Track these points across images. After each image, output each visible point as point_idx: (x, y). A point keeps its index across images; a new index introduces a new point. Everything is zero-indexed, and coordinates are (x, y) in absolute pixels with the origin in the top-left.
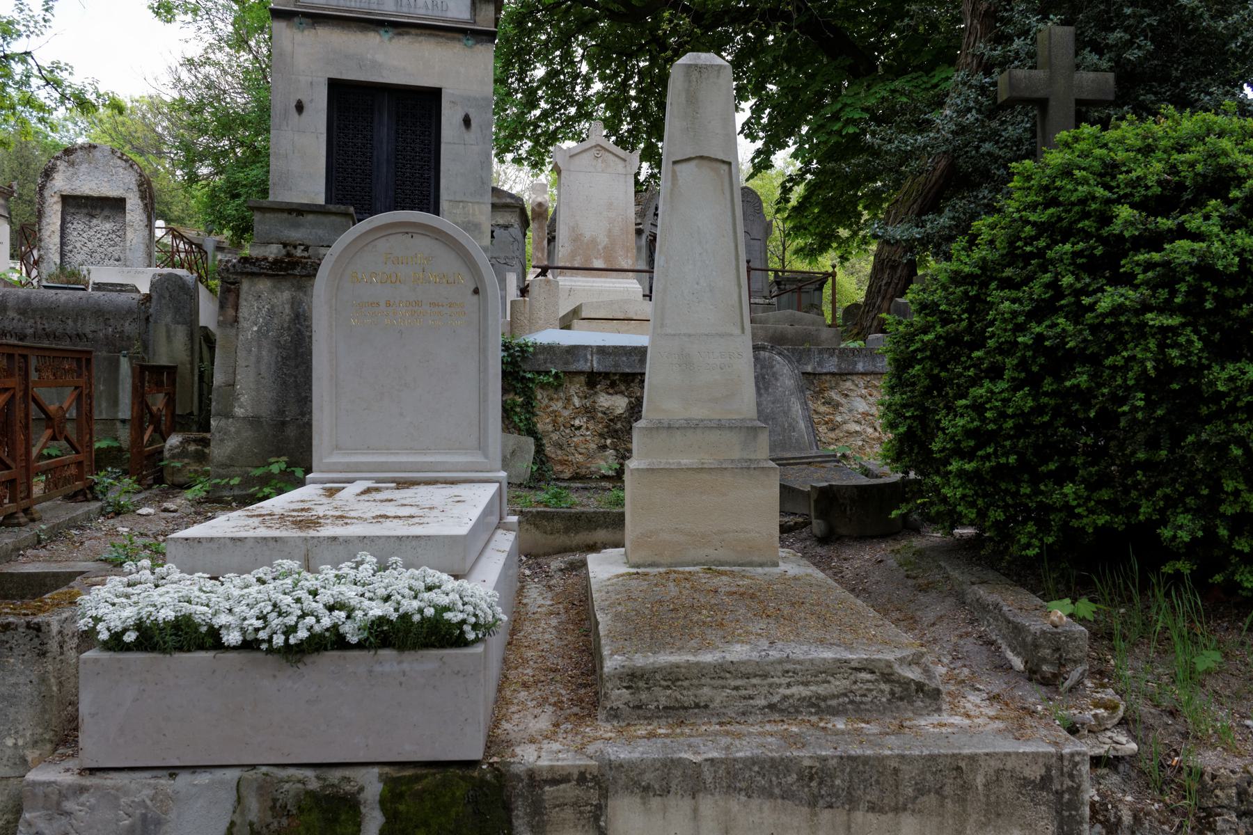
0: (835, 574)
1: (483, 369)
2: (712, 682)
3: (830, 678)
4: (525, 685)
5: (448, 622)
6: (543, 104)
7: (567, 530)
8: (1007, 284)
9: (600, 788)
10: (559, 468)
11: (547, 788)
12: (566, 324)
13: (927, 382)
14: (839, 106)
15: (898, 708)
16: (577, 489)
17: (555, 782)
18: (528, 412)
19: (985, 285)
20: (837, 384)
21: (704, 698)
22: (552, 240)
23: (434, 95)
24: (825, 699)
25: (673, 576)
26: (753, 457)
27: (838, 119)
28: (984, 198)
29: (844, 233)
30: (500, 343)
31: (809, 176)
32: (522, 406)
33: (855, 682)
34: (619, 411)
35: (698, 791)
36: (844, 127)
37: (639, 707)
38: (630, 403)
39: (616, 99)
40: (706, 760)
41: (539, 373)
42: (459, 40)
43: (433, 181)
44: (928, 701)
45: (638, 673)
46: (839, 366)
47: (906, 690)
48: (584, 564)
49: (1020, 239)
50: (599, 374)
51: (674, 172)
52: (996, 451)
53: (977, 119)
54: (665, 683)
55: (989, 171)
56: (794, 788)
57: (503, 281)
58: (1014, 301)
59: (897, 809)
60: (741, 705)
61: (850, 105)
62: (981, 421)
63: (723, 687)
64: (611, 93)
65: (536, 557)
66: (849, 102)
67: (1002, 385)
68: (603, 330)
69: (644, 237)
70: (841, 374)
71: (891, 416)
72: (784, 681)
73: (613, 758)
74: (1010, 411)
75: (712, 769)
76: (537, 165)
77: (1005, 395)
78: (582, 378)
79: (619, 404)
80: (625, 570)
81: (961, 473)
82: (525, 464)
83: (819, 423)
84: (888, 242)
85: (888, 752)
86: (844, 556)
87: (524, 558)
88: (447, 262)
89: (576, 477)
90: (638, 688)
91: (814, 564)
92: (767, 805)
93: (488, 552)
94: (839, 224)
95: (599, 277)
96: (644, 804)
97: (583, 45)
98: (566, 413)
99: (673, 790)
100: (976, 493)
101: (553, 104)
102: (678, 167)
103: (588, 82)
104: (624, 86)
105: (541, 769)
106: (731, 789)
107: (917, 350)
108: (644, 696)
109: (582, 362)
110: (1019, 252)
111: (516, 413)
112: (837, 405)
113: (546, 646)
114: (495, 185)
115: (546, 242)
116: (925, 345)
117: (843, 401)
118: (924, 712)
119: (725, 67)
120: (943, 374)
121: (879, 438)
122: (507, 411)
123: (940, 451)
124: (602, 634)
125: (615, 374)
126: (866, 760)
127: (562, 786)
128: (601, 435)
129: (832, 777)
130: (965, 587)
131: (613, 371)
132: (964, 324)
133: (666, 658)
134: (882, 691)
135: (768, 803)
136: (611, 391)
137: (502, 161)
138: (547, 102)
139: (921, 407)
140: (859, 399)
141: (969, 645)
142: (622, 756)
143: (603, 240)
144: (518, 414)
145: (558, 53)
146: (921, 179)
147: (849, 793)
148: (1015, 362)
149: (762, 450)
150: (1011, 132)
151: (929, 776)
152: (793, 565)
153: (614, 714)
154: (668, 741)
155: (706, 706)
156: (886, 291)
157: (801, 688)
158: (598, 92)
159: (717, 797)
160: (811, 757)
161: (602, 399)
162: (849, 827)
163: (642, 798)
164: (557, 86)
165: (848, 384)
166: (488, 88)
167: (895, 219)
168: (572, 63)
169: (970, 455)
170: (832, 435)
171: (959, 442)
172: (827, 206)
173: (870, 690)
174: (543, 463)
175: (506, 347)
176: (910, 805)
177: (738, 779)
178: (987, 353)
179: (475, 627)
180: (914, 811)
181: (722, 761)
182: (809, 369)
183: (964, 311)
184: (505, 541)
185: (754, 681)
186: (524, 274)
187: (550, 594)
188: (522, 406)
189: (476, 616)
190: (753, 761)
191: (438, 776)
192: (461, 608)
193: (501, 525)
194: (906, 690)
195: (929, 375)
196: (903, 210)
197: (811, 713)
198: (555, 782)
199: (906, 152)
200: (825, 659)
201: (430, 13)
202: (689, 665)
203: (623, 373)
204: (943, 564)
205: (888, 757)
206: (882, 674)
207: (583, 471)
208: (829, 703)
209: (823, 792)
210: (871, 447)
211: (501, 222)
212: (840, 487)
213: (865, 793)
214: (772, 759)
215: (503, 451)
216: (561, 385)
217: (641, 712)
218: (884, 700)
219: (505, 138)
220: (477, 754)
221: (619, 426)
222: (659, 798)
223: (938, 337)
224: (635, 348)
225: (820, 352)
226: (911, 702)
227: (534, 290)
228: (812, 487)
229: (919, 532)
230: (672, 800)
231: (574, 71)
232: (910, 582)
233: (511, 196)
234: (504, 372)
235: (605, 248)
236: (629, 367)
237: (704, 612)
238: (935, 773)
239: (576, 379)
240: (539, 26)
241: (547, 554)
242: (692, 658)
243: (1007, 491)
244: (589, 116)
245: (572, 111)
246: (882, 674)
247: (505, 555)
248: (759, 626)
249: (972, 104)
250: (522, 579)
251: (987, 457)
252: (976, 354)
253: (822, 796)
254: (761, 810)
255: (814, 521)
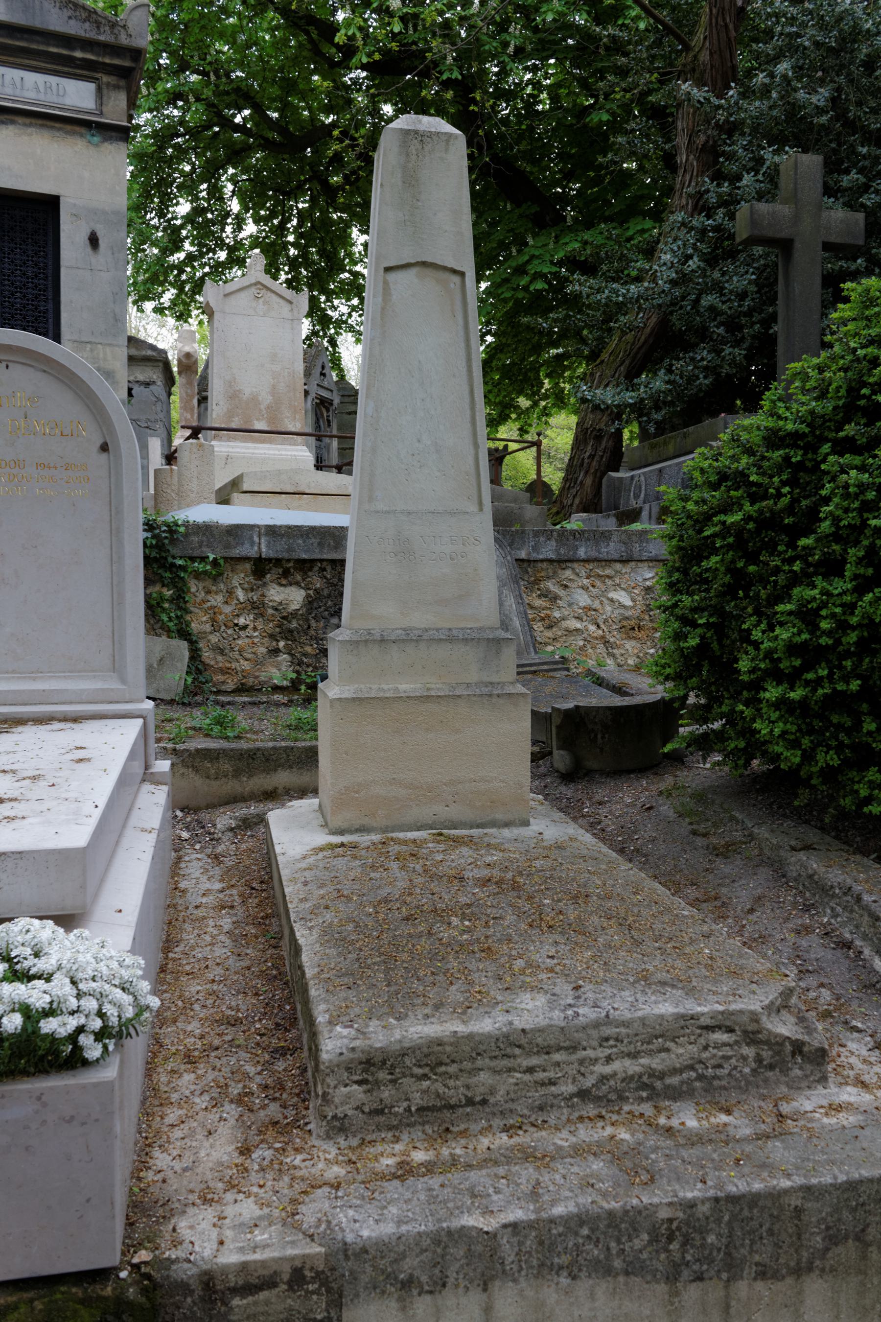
0: (592, 825)
1: (116, 558)
2: (493, 1064)
3: (670, 1044)
4: (190, 1059)
5: (52, 1038)
6: (187, 246)
7: (237, 774)
8: (845, 446)
9: (329, 1290)
10: (220, 678)
11: (236, 1302)
12: (223, 498)
13: (727, 579)
14: (526, 258)
15: (766, 1081)
16: (244, 705)
17: (249, 1289)
18: (180, 608)
19: (812, 448)
20: (555, 573)
21: (482, 1089)
22: (203, 400)
23: (50, 205)
24: (662, 1076)
25: (394, 849)
26: (495, 679)
27: (525, 272)
28: (702, 359)
29: (524, 402)
30: (141, 521)
31: (489, 339)
32: (171, 601)
33: (706, 1048)
34: (294, 606)
35: (493, 1278)
36: (531, 282)
37: (379, 1112)
38: (308, 596)
39: (273, 244)
40: (505, 1226)
41: (193, 559)
42: (82, 136)
43: (51, 316)
44: (809, 1067)
45: (378, 1059)
46: (557, 551)
47: (778, 1053)
48: (262, 820)
49: (865, 384)
50: (269, 560)
51: (386, 283)
52: (830, 675)
53: (699, 267)
54: (418, 1071)
55: (705, 329)
56: (645, 1256)
57: (144, 448)
58: (862, 469)
59: (799, 1271)
60: (536, 1095)
61: (538, 257)
62: (812, 633)
63: (510, 1070)
64: (267, 237)
65: (196, 810)
66: (537, 253)
67: (839, 586)
68: (269, 506)
69: (310, 399)
70: (559, 561)
71: (676, 625)
72: (602, 1053)
73: (350, 1238)
74: (854, 620)
75: (515, 1240)
76: (183, 317)
77: (847, 598)
78: (248, 566)
79: (293, 597)
80: (323, 838)
81: (781, 704)
82: (176, 677)
83: (534, 620)
84: (597, 407)
85: (786, 1183)
86: (597, 798)
87: (179, 814)
88: (61, 405)
89: (242, 689)
90: (377, 1083)
91: (561, 810)
92: (602, 1288)
93: (129, 833)
94: (520, 393)
95: (271, 442)
96: (403, 1309)
97: (233, 180)
98: (227, 609)
99: (451, 1281)
100: (800, 730)
101: (200, 245)
102: (392, 277)
103: (239, 224)
104: (281, 229)
105: (225, 1270)
106: (545, 1269)
107: (714, 535)
108: (386, 1093)
109: (247, 545)
110: (862, 402)
111: (164, 610)
112: (555, 598)
113: (219, 970)
114: (133, 333)
115: (195, 402)
116: (726, 529)
117: (561, 593)
118: (804, 1084)
119: (456, 137)
120: (752, 568)
121: (603, 637)
122: (152, 608)
123: (750, 672)
124: (309, 973)
125: (288, 561)
126: (753, 1200)
127: (263, 1295)
128: (272, 636)
129: (703, 1231)
130: (782, 853)
131: (286, 556)
132: (784, 501)
133: (419, 1029)
134: (744, 1058)
135: (604, 1285)
136: (284, 582)
137: (141, 310)
138: (192, 244)
139: (718, 610)
140: (580, 591)
141: (816, 948)
142: (365, 1233)
143: (266, 399)
144: (166, 611)
145: (205, 186)
146: (629, 337)
147: (728, 1254)
148: (861, 553)
149: (505, 669)
150: (737, 283)
151: (846, 1215)
152: (549, 827)
153: (339, 1127)
154: (435, 1182)
155: (484, 1102)
156: (590, 464)
157: (627, 1062)
158: (251, 236)
159: (523, 1284)
160: (670, 1204)
161: (272, 592)
162: (728, 1307)
163: (400, 1299)
164: (204, 225)
165: (568, 573)
166: (121, 201)
167: (600, 383)
168: (221, 199)
169: (792, 679)
170: (549, 634)
171: (779, 660)
172: (506, 372)
173: (727, 1058)
174: (199, 672)
175: (149, 526)
176: (817, 1263)
177: (555, 1250)
178: (817, 540)
179: (99, 1036)
180: (823, 1270)
181: (531, 1225)
182: (523, 555)
183: (784, 483)
184: (153, 804)
185: (557, 1057)
186: (170, 441)
187: (217, 871)
188: (171, 601)
189: (101, 1014)
190: (580, 1219)
191: (39, 1305)
192: (73, 1003)
193: (148, 777)
194: (778, 1053)
195: (731, 570)
196: (608, 373)
197: (642, 1100)
198: (249, 1289)
199: (617, 303)
200: (662, 1017)
201: (42, 97)
202: (457, 1040)
203: (314, 564)
204: (739, 815)
205: (786, 1192)
206: (745, 1032)
207: (250, 681)
208: (668, 1081)
209: (688, 1257)
210: (594, 648)
211: (141, 378)
212: (589, 710)
213: (752, 1251)
214: (611, 1214)
215: (147, 658)
216: (221, 574)
217: (382, 1119)
218: (747, 1070)
219: (145, 282)
220: (115, 1259)
221: (294, 624)
222: (428, 1298)
223: (748, 518)
224: (313, 528)
225: (536, 534)
226: (785, 1071)
227: (183, 457)
228: (553, 708)
229: (683, 763)
230: (449, 1298)
231: (223, 209)
232: (699, 841)
233: (153, 348)
234: (146, 558)
235: (268, 407)
236: (306, 552)
237: (455, 921)
238: (855, 1210)
239: (240, 567)
240: (181, 153)
241: (212, 806)
242: (461, 1028)
243: (840, 727)
244: (241, 263)
245: (222, 255)
246: (745, 1032)
247: (153, 837)
248: (542, 950)
249: (690, 251)
250: (178, 846)
251: (818, 682)
252: (803, 542)
253: (687, 1264)
254: (592, 1297)
255: (556, 752)
